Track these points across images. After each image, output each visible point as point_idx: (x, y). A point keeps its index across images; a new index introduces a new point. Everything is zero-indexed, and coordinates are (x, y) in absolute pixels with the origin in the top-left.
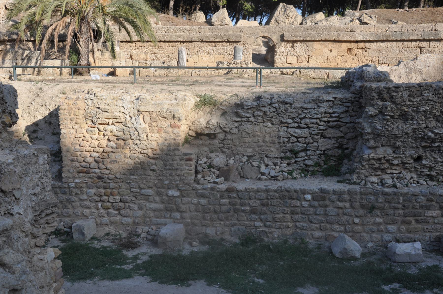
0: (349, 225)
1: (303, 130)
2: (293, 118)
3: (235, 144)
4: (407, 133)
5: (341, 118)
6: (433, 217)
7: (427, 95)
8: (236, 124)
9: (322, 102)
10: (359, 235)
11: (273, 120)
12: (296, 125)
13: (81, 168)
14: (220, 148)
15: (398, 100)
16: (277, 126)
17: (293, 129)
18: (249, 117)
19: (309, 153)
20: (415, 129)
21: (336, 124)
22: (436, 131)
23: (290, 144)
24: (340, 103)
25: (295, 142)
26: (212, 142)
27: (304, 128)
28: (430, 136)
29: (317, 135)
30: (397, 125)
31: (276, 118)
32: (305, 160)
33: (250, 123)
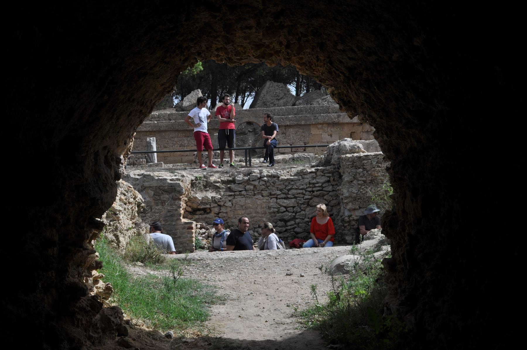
2: (281, 190)
8: (230, 198)
9: (306, 173)
11: (262, 192)
15: (368, 167)
18: (241, 191)
19: (297, 221)
23: (280, 214)
25: (284, 212)
26: (208, 216)
27: (291, 198)
32: (294, 228)
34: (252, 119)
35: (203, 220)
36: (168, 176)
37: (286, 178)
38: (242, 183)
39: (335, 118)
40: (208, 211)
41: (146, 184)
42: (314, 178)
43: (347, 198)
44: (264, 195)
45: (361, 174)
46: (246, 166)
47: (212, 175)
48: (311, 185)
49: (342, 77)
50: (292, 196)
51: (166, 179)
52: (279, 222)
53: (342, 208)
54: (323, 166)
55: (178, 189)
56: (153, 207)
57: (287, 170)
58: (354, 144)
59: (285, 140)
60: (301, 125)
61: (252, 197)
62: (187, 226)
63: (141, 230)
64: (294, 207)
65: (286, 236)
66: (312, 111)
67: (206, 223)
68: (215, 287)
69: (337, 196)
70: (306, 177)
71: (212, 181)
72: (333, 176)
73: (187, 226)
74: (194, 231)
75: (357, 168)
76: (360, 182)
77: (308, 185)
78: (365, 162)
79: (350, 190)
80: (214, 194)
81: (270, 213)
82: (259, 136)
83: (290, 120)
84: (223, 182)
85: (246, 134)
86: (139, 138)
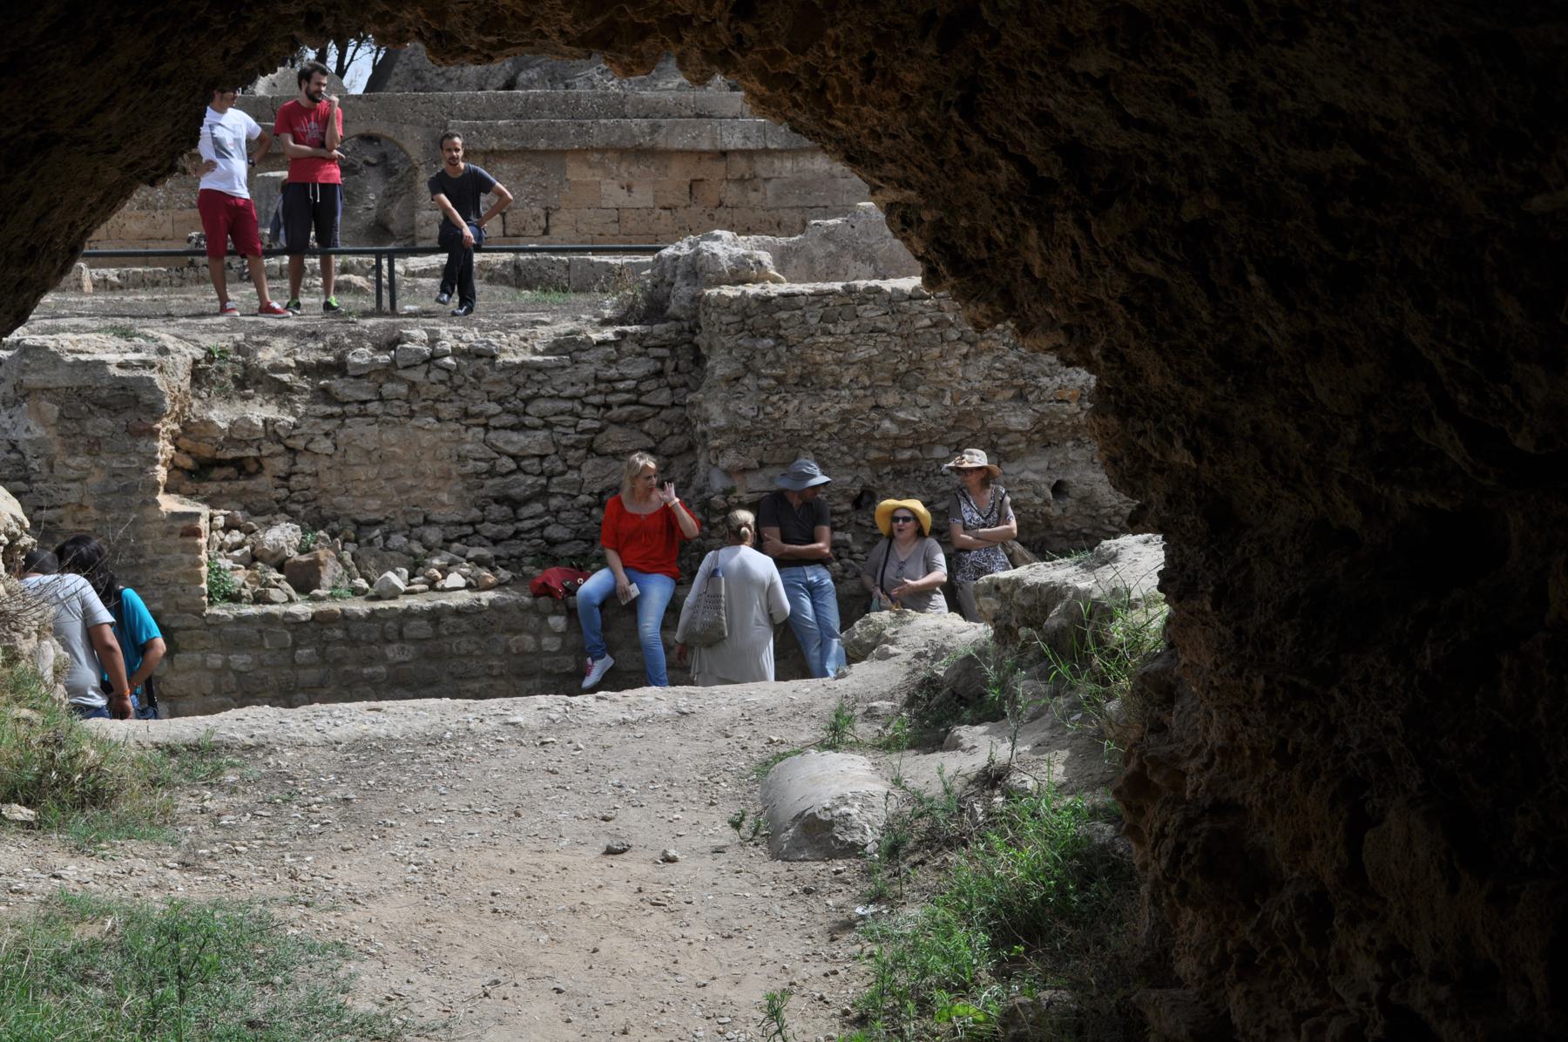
2: (500, 401)
3: (325, 486)
4: (824, 426)
8: (327, 426)
9: (586, 346)
11: (440, 406)
12: (509, 419)
14: (278, 501)
15: (792, 334)
16: (454, 426)
17: (502, 433)
18: (364, 402)
19: (555, 502)
20: (844, 411)
21: (631, 413)
22: (902, 415)
23: (497, 480)
25: (511, 472)
26: (251, 484)
27: (535, 428)
28: (888, 430)
29: (577, 449)
30: (796, 402)
31: (451, 401)
32: (542, 527)
33: (371, 420)
34: (380, 128)
35: (236, 497)
36: (109, 352)
37: (517, 360)
38: (368, 375)
39: (643, 134)
40: (253, 467)
41: (32, 379)
42: (610, 362)
43: (720, 432)
44: (444, 415)
45: (771, 357)
46: (378, 312)
47: (265, 344)
48: (602, 386)
49: (1005, 172)
50: (538, 422)
51: (103, 363)
52: (494, 507)
53: (702, 461)
54: (640, 322)
55: (147, 397)
56: (57, 461)
57: (522, 332)
58: (740, 251)
60: (536, 152)
61: (402, 424)
62: (179, 525)
63: (19, 636)
64: (542, 457)
65: (515, 551)
66: (572, 109)
67: (246, 508)
68: (342, 950)
69: (686, 422)
70: (584, 356)
72: (674, 356)
73: (179, 525)
74: (203, 541)
75: (756, 334)
76: (764, 383)
77: (591, 387)
78: (784, 315)
79: (732, 406)
80: (271, 412)
81: (463, 477)
82: (401, 180)
83: (500, 135)
84: (303, 369)
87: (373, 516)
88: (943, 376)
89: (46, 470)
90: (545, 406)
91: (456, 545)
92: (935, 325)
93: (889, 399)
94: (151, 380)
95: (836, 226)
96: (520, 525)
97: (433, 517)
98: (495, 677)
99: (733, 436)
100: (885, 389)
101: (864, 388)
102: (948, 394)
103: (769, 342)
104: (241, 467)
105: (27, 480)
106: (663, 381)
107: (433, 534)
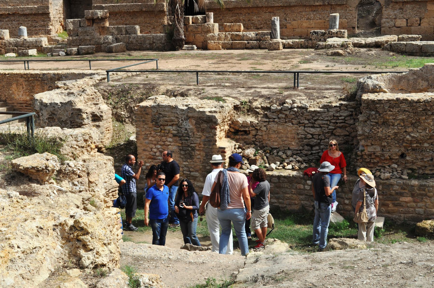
0: (342, 205)
1: (316, 129)
2: (308, 120)
4: (389, 136)
5: (346, 120)
6: (405, 202)
7: (403, 106)
9: (331, 107)
10: (348, 213)
11: (293, 121)
12: (310, 125)
13: (150, 156)
14: (253, 141)
17: (309, 128)
19: (322, 147)
20: (395, 132)
22: (412, 135)
23: (307, 140)
24: (345, 108)
25: (310, 138)
27: (318, 127)
30: (381, 129)
32: (319, 153)
38: (275, 112)
40: (248, 132)
41: (190, 115)
42: (337, 112)
43: (360, 135)
44: (294, 123)
48: (335, 118)
50: (318, 126)
55: (214, 120)
56: (195, 133)
59: (402, 15)
62: (221, 150)
64: (319, 135)
70: (330, 110)
71: (254, 107)
75: (371, 110)
76: (372, 123)
77: (332, 118)
78: (378, 105)
79: (364, 128)
81: (298, 139)
84: (263, 108)
85: (373, 4)
86: (273, 12)
87: (275, 147)
88: (426, 124)
89: (193, 135)
90: (320, 122)
91: (295, 156)
92: (424, 110)
93: (409, 130)
94: (215, 116)
95: (417, 70)
96: (312, 152)
97: (290, 148)
98: (293, 194)
99: (363, 137)
100: (409, 127)
101: (402, 126)
102: (428, 129)
103: (373, 112)
104: (246, 133)
105: (189, 137)
106: (352, 117)
107: (289, 153)
